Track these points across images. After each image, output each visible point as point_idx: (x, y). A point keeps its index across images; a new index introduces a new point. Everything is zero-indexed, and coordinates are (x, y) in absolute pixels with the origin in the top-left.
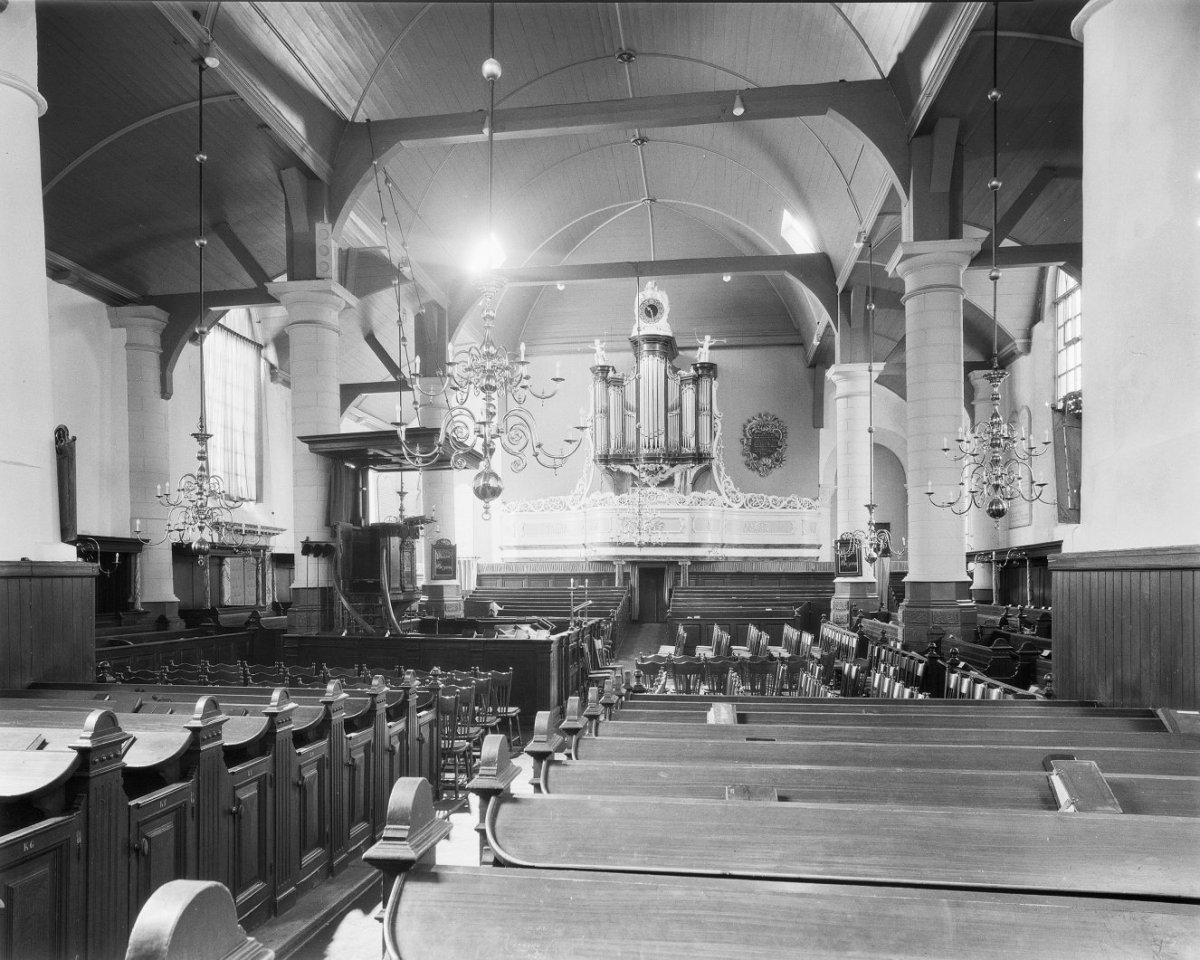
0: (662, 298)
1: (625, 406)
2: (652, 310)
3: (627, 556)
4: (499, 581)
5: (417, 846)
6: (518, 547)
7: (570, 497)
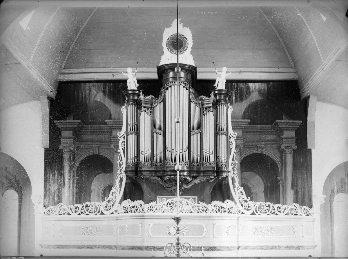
1: (153, 125)
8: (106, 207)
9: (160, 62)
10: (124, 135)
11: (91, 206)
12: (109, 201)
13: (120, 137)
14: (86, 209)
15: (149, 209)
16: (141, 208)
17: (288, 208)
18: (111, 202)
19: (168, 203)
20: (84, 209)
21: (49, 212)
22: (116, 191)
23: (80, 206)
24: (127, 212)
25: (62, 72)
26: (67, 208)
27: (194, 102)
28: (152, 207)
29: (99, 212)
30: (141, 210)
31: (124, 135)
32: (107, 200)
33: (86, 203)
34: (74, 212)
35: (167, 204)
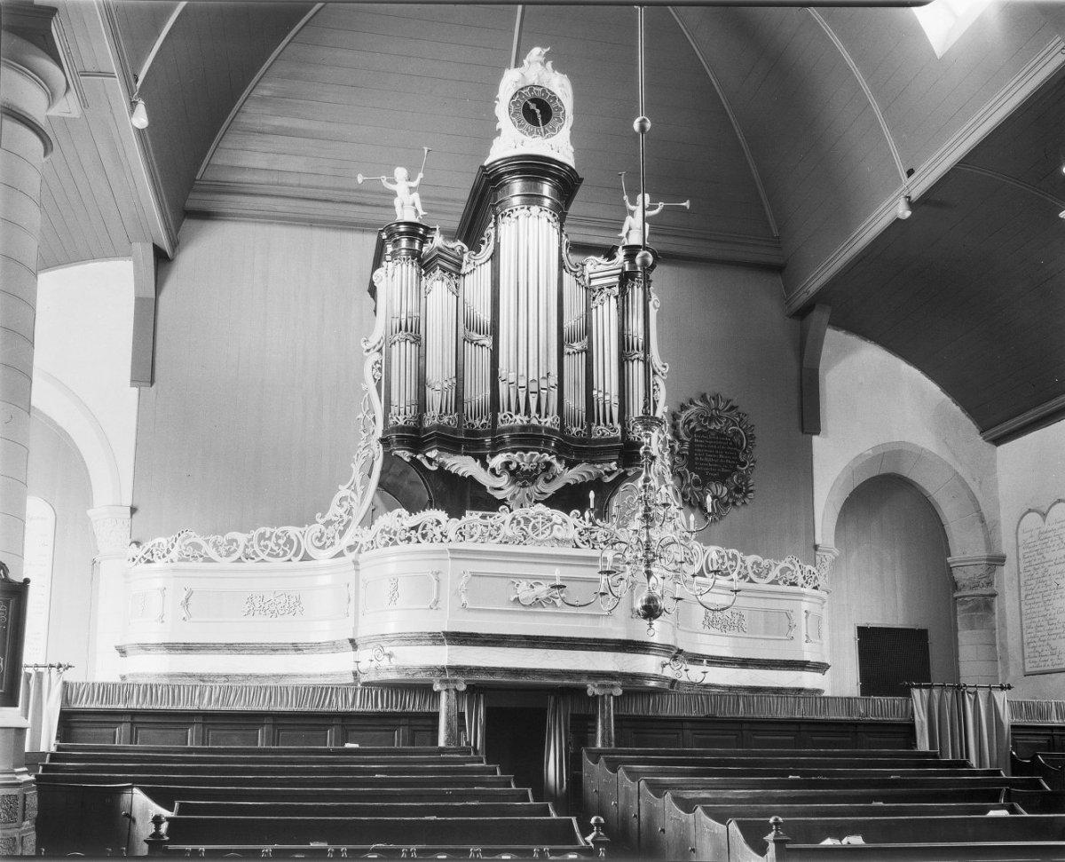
0: (560, 86)
2: (537, 110)
3: (478, 670)
4: (121, 731)
5: (99, 687)
6: (171, 647)
7: (315, 529)
8: (320, 539)
9: (487, 154)
10: (379, 343)
11: (274, 538)
12: (329, 523)
13: (368, 351)
14: (260, 546)
15: (461, 533)
16: (437, 531)
17: (776, 565)
18: (336, 525)
19: (514, 519)
20: (252, 546)
21: (149, 553)
22: (353, 495)
23: (242, 538)
24: (396, 543)
25: (190, 204)
26: (204, 544)
27: (571, 271)
28: (471, 529)
29: (296, 555)
30: (439, 537)
31: (379, 343)
32: (323, 521)
33: (262, 530)
34: (224, 553)
35: (512, 522)
